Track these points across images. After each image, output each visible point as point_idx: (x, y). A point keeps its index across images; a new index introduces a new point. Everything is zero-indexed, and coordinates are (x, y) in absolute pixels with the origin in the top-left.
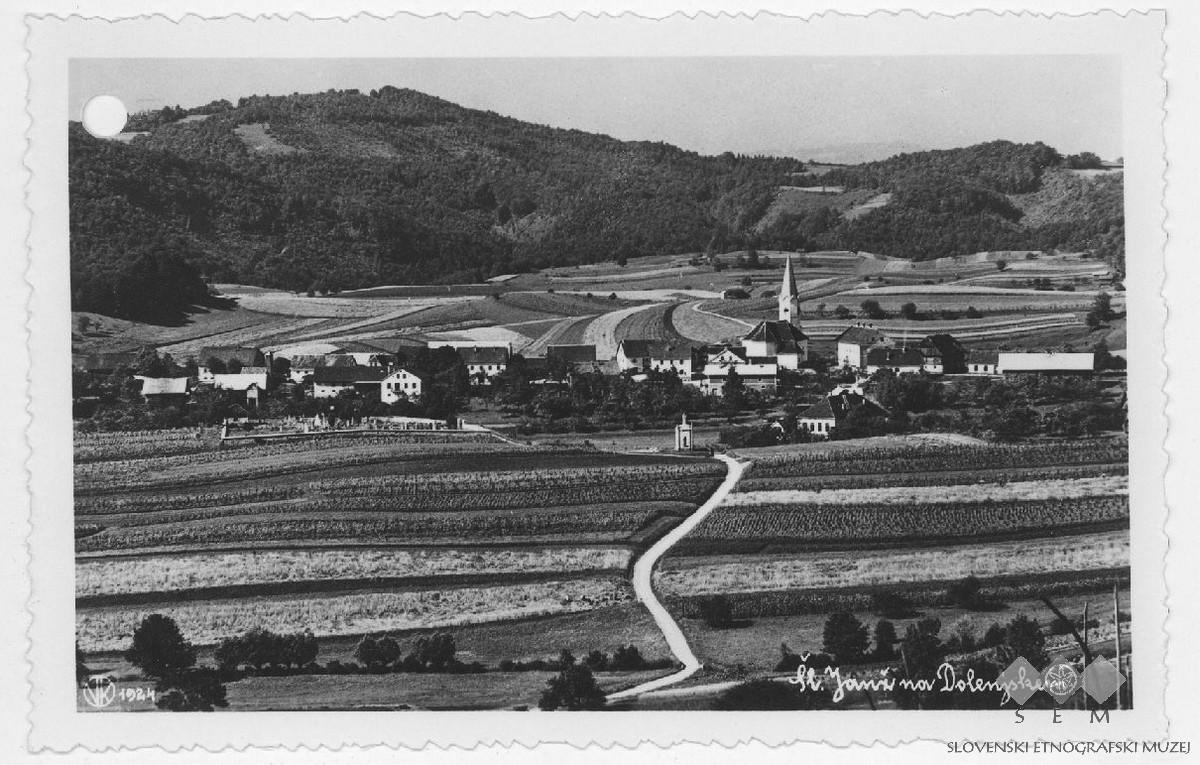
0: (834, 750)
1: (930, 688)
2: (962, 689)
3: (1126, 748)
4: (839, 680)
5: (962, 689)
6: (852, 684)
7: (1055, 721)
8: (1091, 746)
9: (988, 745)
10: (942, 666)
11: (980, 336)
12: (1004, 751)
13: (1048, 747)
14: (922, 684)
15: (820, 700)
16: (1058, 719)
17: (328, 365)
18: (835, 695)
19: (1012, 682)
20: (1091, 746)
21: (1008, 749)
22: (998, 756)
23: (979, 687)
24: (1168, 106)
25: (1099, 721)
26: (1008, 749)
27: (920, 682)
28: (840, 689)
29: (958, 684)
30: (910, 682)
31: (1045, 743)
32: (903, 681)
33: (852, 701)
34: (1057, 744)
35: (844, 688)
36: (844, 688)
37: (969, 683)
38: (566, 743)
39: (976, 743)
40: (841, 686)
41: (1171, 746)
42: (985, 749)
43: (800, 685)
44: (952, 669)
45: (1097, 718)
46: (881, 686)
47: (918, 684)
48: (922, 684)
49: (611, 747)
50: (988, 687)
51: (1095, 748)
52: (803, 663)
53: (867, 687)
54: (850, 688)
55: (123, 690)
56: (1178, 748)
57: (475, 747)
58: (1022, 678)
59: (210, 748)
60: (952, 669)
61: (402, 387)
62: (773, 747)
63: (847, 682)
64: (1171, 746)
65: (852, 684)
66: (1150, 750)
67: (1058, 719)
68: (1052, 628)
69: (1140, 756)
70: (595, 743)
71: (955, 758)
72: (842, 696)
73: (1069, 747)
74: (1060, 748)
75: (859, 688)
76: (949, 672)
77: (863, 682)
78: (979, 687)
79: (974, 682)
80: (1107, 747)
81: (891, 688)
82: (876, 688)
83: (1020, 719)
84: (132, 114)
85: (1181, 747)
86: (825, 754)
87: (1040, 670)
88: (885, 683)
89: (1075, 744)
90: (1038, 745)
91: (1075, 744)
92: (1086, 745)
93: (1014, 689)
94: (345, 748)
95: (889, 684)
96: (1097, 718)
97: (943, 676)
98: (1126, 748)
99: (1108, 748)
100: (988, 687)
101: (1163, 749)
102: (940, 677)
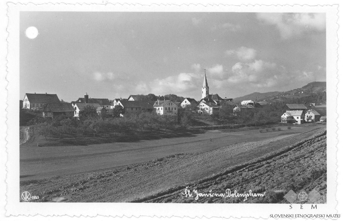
2: (233, 196)
3: (322, 216)
4: (197, 194)
6: (201, 195)
7: (301, 208)
8: (311, 215)
10: (227, 190)
12: (286, 217)
16: (302, 208)
19: (247, 194)
20: (311, 215)
21: (287, 216)
23: (238, 195)
25: (314, 208)
26: (287, 216)
27: (220, 194)
28: (197, 196)
31: (298, 215)
33: (202, 200)
36: (199, 196)
37: (235, 194)
41: (335, 216)
49: (29, 216)
50: (240, 196)
51: (313, 216)
53: (241, 196)
58: (250, 193)
60: (230, 190)
61: (171, 109)
64: (335, 216)
65: (201, 195)
67: (302, 208)
68: (308, 181)
73: (305, 216)
75: (203, 196)
80: (316, 216)
88: (210, 194)
89: (307, 215)
91: (307, 215)
92: (310, 215)
93: (248, 196)
100: (240, 196)
101: (332, 216)
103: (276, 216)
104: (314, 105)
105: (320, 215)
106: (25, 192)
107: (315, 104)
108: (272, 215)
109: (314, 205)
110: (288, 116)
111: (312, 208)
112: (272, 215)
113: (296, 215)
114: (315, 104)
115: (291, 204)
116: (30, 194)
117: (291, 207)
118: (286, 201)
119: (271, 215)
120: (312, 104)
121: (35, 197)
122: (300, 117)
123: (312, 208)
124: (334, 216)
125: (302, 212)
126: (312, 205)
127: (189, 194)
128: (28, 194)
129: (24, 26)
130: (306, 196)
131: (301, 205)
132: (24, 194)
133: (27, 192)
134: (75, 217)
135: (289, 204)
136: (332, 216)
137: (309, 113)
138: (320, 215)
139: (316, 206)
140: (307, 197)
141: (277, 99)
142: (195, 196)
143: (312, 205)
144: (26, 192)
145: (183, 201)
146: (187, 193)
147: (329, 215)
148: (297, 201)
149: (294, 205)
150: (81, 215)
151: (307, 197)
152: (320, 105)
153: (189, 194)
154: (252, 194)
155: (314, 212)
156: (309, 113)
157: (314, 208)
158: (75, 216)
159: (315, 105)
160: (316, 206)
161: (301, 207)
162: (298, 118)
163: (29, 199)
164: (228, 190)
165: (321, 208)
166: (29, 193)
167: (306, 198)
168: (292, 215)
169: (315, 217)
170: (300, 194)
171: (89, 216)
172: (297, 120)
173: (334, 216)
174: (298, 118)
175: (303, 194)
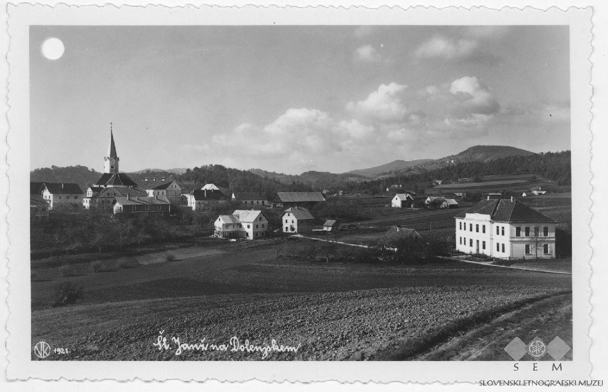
5: (243, 350)
6: (186, 346)
7: (534, 370)
8: (552, 382)
9: (500, 382)
10: (231, 339)
11: (462, 182)
14: (222, 347)
15: (168, 356)
16: (536, 369)
17: (393, 87)
18: (177, 351)
20: (552, 382)
21: (510, 384)
22: (506, 388)
24: (593, 100)
25: (557, 369)
30: (216, 346)
32: (212, 346)
33: (186, 357)
34: (535, 381)
35: (182, 348)
36: (182, 348)
37: (247, 347)
42: (499, 383)
45: (556, 368)
48: (222, 347)
51: (555, 384)
52: (160, 335)
54: (185, 349)
56: (597, 383)
57: (283, 382)
58: (273, 345)
63: (183, 345)
65: (186, 346)
66: (582, 385)
67: (536, 369)
70: (137, 378)
71: (483, 388)
74: (537, 383)
75: (189, 348)
76: (236, 341)
79: (249, 348)
81: (206, 349)
82: (198, 349)
85: (598, 383)
86: (335, 386)
87: (527, 344)
88: (202, 346)
90: (525, 382)
92: (550, 382)
94: (208, 381)
95: (205, 346)
96: (556, 368)
99: (561, 383)
102: (231, 344)
103: (490, 383)
104: (439, 184)
105: (568, 382)
106: (41, 343)
107: (441, 181)
108: (482, 382)
109: (557, 363)
110: (224, 223)
111: (553, 370)
112: (482, 382)
113: (525, 382)
114: (441, 181)
115: (516, 362)
116: (49, 346)
117: (517, 367)
118: (510, 357)
119: (481, 382)
120: (436, 181)
121: (60, 351)
122: (251, 225)
123: (553, 370)
124: (593, 383)
125: (536, 376)
126: (554, 365)
127: (164, 344)
128: (46, 346)
129: (38, 34)
130: (543, 348)
131: (534, 364)
132: (39, 346)
133: (44, 343)
134: (63, 379)
135: (513, 363)
136: (589, 383)
137: (289, 215)
138: (568, 382)
139: (560, 365)
140: (545, 350)
141: (411, 172)
142: (174, 347)
143: (554, 365)
144: (42, 343)
145: (214, 358)
146: (162, 342)
147: (583, 382)
148: (547, 357)
149: (540, 364)
150: (371, 380)
151: (545, 350)
152: (450, 183)
153: (164, 344)
154: (277, 346)
155: (558, 375)
156: (289, 215)
157: (557, 369)
158: (88, 379)
159: (442, 183)
160: (560, 365)
161: (534, 367)
162: (249, 227)
163: (48, 355)
164: (233, 339)
165: (569, 370)
166: (47, 344)
167: (543, 352)
168: (574, 382)
169: (558, 384)
170: (531, 345)
171: (156, 380)
172: (247, 230)
173: (593, 383)
174: (249, 227)
175: (538, 345)
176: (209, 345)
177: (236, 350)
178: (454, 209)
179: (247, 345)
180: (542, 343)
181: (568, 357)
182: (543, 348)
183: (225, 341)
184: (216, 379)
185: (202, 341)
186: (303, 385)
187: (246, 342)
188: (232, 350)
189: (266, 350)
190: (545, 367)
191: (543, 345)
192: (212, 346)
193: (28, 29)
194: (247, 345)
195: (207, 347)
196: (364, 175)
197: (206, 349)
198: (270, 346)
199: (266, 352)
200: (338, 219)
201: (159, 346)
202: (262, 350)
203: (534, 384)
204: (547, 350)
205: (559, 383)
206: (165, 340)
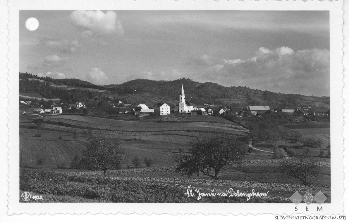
0: (205, 216)
1: (226, 196)
3: (327, 218)
5: (236, 196)
6: (203, 194)
7: (306, 210)
8: (317, 217)
10: (230, 189)
12: (292, 219)
13: (305, 217)
14: (224, 195)
18: (198, 198)
20: (317, 217)
21: (293, 218)
25: (320, 210)
26: (293, 218)
28: (200, 196)
29: (235, 194)
31: (304, 217)
32: (218, 194)
35: (201, 195)
36: (201, 195)
37: (238, 194)
38: (101, 213)
39: (283, 217)
40: (200, 195)
41: (341, 217)
43: (188, 195)
44: (232, 190)
45: (319, 209)
46: (212, 195)
47: (223, 195)
51: (318, 218)
54: (203, 196)
55: (34, 196)
56: (342, 218)
58: (253, 193)
59: (149, 214)
60: (232, 190)
62: (39, 215)
63: (202, 194)
64: (341, 217)
65: (203, 194)
66: (334, 219)
69: (332, 220)
72: (200, 198)
73: (311, 218)
75: (205, 196)
76: (232, 190)
77: (207, 194)
78: (240, 195)
81: (215, 196)
82: (210, 196)
83: (296, 210)
84: (21, 72)
85: (343, 218)
88: (213, 194)
92: (316, 217)
95: (214, 194)
96: (319, 209)
97: (230, 192)
98: (327, 218)
105: (326, 217)
111: (317, 210)
113: (302, 217)
119: (276, 217)
123: (317, 210)
124: (340, 218)
125: (308, 214)
126: (318, 207)
131: (307, 207)
136: (338, 218)
137: (188, 111)
139: (322, 208)
142: (197, 195)
143: (318, 207)
146: (190, 193)
147: (334, 217)
153: (191, 193)
157: (320, 210)
160: (322, 208)
161: (307, 209)
170: (305, 196)
176: (217, 194)
177: (232, 196)
178: (55, 99)
179: (238, 193)
180: (311, 195)
181: (328, 201)
182: (312, 198)
183: (225, 189)
184: (201, 213)
185: (213, 191)
186: (244, 216)
187: (253, 191)
188: (230, 196)
189: (249, 195)
190: (313, 207)
191: (312, 196)
192: (218, 194)
193: (326, 9)
194: (238, 193)
195: (215, 195)
196: (48, 74)
197: (215, 196)
198: (252, 193)
199: (249, 196)
200: (235, 115)
201: (188, 195)
202: (246, 196)
203: (307, 217)
204: (314, 198)
205: (321, 218)
206: (191, 191)
